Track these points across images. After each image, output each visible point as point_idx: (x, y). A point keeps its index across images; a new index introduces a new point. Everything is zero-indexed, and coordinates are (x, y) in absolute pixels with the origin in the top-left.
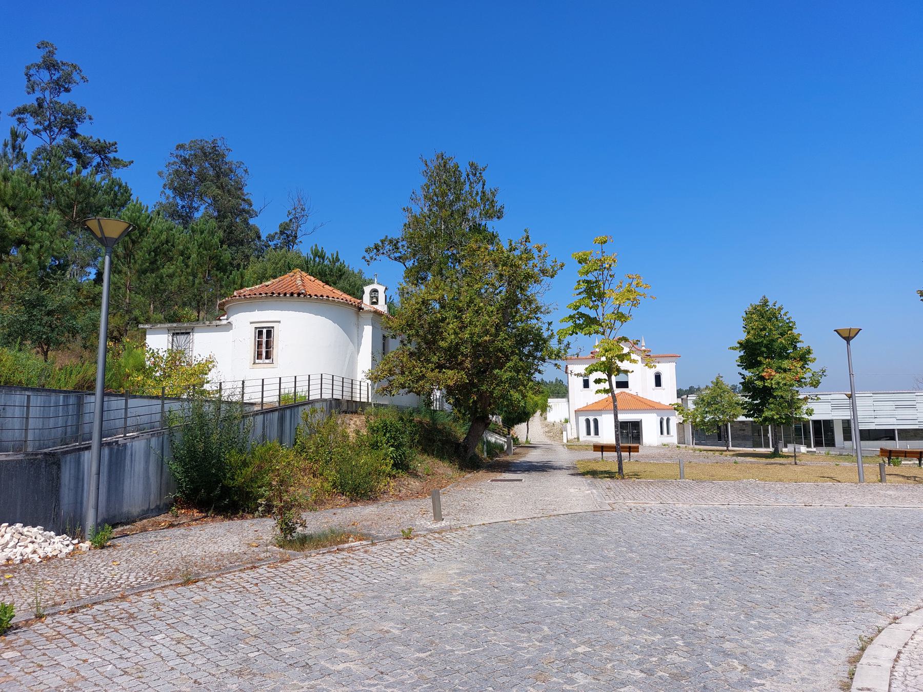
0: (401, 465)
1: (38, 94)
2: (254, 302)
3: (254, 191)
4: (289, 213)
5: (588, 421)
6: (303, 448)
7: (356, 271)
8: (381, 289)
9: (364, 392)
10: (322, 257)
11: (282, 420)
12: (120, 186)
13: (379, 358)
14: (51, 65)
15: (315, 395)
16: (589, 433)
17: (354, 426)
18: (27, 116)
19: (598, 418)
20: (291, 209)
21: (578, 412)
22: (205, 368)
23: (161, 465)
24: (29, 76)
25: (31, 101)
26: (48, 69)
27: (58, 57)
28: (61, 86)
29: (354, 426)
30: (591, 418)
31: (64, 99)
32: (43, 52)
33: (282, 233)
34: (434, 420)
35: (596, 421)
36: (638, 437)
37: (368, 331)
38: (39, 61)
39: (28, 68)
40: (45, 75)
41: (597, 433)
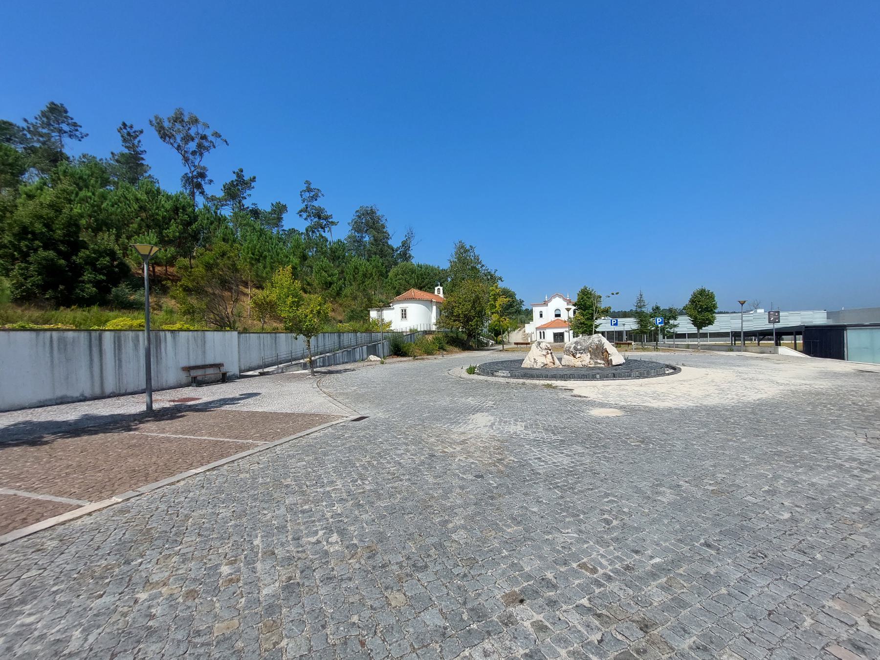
0: (442, 348)
1: (306, 203)
2: (399, 302)
3: (389, 229)
4: (406, 236)
5: (540, 332)
6: (417, 344)
7: (436, 267)
8: (441, 288)
9: (434, 328)
10: (421, 267)
11: (411, 337)
12: (341, 242)
13: (438, 317)
14: (309, 190)
15: (419, 330)
16: (541, 338)
17: (430, 338)
18: (302, 213)
19: (545, 331)
20: (406, 233)
21: (537, 329)
22: (390, 323)
23: (389, 348)
24: (301, 195)
25: (303, 206)
26: (308, 191)
27: (312, 187)
28: (315, 198)
29: (430, 338)
30: (542, 331)
31: (316, 204)
32: (306, 185)
33: (403, 246)
34: (457, 336)
35: (544, 332)
36: (562, 340)
37: (434, 308)
38: (305, 189)
39: (301, 192)
40: (307, 194)
41: (544, 338)
